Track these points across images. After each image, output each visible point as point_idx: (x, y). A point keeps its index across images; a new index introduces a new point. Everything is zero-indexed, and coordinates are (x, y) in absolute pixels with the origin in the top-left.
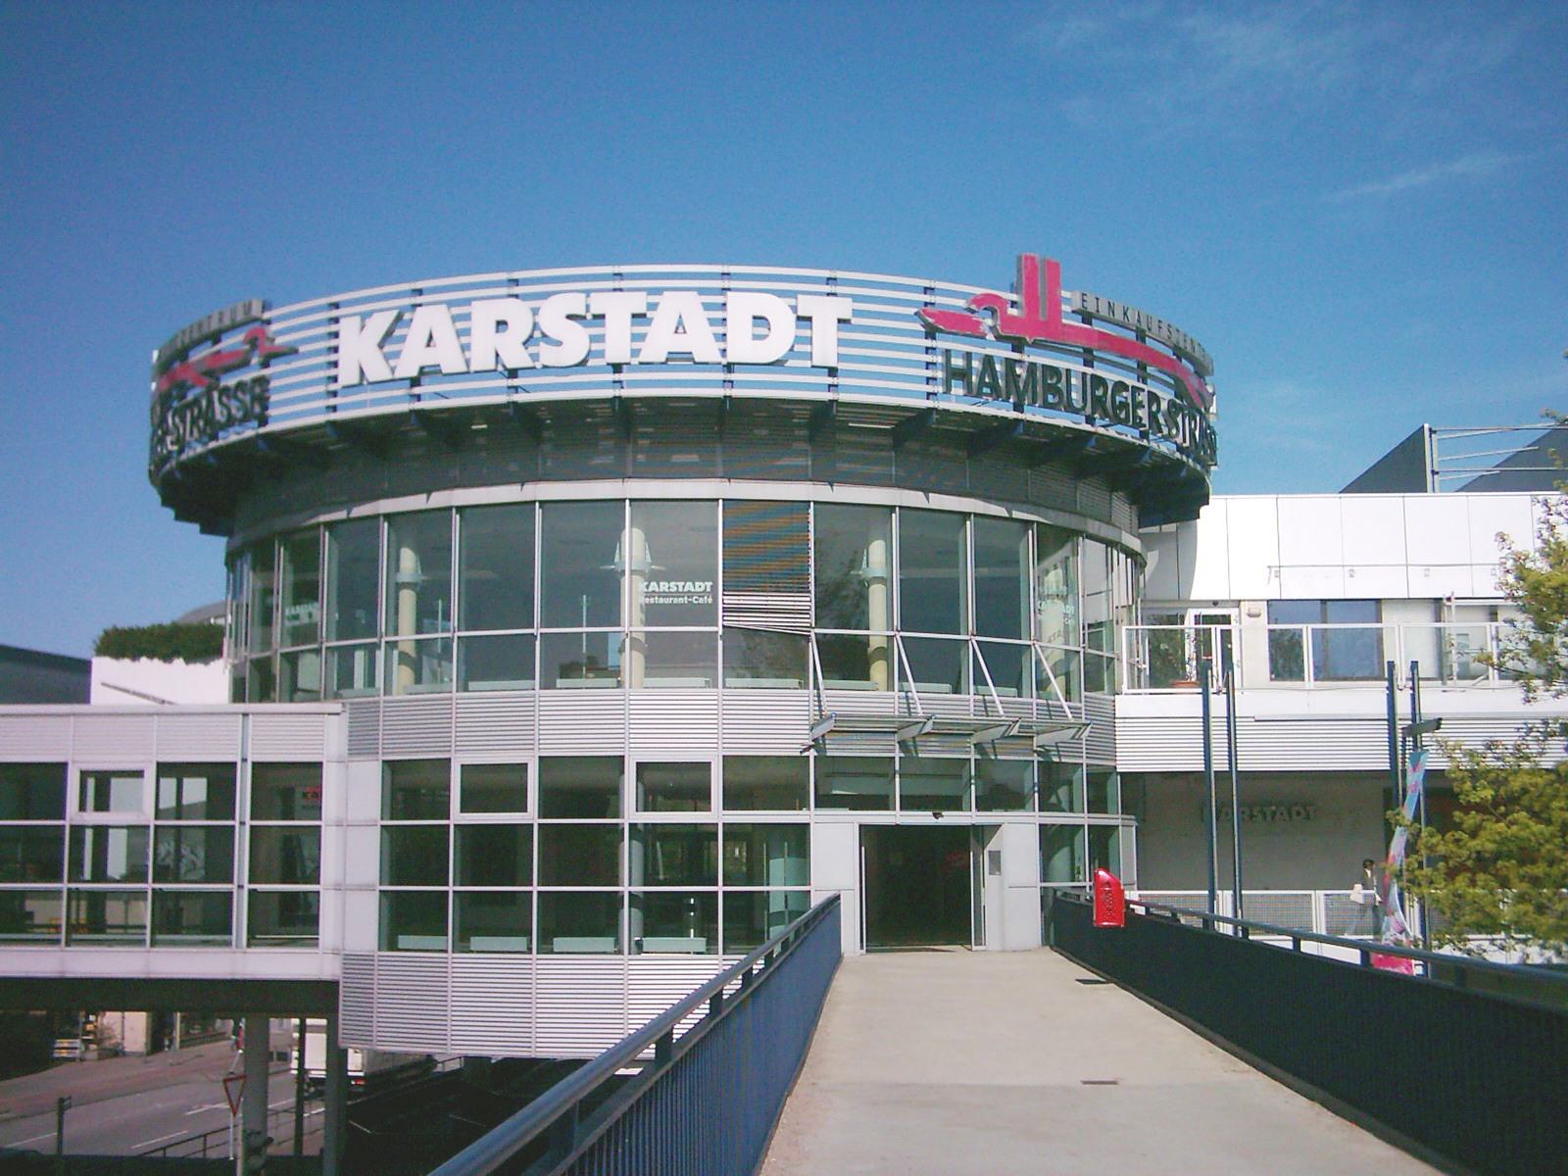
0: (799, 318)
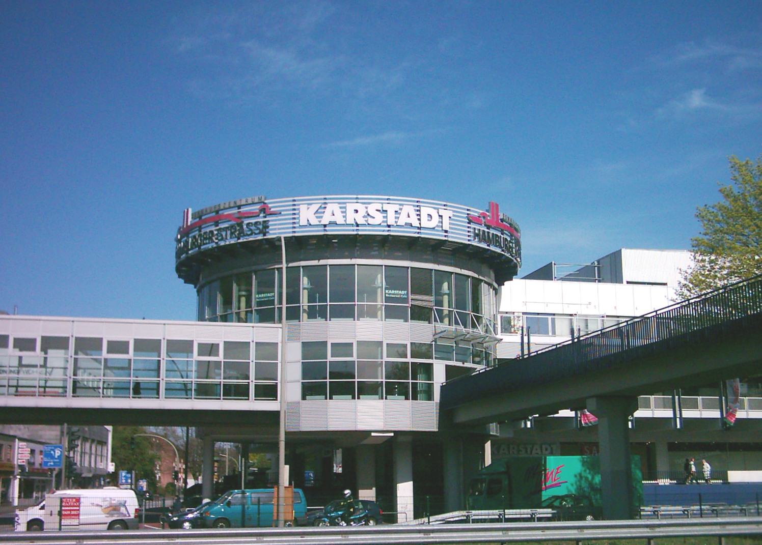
0: (439, 216)
